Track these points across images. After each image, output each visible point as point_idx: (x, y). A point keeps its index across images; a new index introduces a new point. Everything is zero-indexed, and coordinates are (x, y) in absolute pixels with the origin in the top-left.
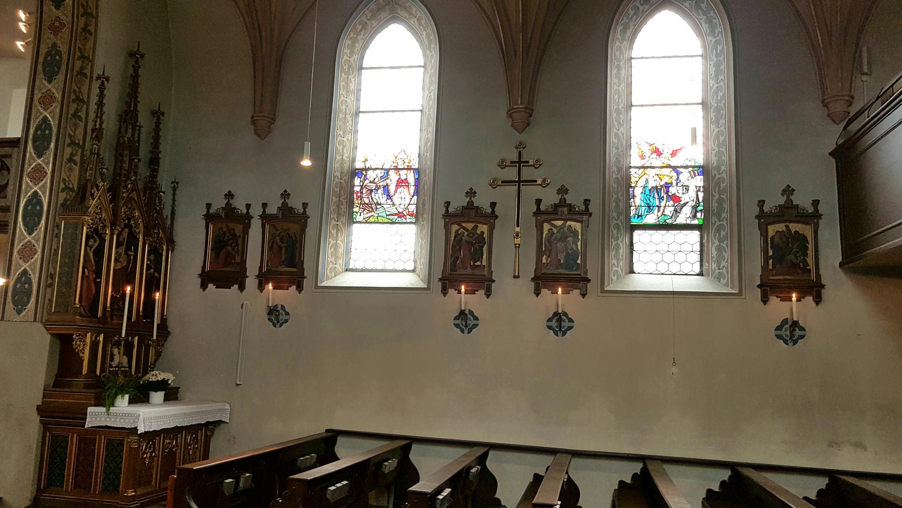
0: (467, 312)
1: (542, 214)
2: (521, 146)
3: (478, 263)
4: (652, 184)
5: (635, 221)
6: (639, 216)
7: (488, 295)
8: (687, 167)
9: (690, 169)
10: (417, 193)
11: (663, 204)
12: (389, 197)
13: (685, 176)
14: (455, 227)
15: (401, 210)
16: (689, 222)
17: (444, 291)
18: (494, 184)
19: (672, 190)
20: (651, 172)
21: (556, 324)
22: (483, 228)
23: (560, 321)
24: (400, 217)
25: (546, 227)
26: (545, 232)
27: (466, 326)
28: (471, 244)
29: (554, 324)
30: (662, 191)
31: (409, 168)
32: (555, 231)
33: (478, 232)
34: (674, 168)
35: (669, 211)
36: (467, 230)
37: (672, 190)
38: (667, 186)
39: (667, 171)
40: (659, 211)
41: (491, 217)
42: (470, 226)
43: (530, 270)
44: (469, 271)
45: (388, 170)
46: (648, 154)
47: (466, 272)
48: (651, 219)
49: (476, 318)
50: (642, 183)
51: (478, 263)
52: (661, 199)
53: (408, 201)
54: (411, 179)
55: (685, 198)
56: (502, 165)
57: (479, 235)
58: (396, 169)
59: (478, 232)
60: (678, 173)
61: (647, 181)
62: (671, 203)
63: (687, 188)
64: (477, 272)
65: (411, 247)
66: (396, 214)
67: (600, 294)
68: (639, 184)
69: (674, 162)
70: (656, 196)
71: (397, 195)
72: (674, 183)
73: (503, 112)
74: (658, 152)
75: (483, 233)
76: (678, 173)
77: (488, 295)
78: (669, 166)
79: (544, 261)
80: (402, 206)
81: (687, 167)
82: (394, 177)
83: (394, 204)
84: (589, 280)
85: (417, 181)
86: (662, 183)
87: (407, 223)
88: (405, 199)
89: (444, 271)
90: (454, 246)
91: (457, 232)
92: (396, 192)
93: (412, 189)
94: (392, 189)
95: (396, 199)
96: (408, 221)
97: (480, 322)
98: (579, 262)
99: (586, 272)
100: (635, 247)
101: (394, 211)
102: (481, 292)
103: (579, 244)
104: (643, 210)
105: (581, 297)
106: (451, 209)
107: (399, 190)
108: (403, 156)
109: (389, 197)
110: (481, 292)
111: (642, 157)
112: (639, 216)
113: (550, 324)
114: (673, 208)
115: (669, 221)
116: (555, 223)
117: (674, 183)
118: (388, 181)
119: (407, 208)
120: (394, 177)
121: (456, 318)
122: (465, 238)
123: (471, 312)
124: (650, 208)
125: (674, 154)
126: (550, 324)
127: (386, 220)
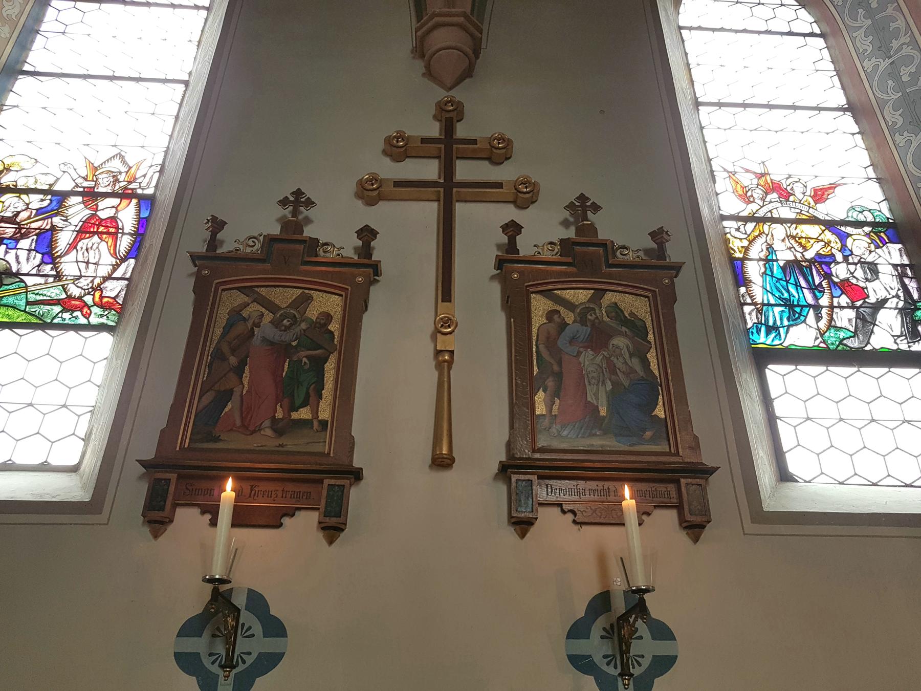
0: (240, 601)
1: (516, 275)
2: (449, 116)
3: (304, 414)
4: (784, 255)
5: (763, 340)
6: (769, 330)
7: (333, 529)
8: (858, 224)
9: (867, 229)
10: (135, 251)
11: (824, 301)
12: (49, 255)
13: (859, 243)
14: (232, 300)
15: (75, 291)
16: (904, 346)
17: (157, 516)
18: (371, 191)
19: (840, 271)
20: (779, 231)
21: (607, 648)
22: (327, 304)
23: (620, 634)
24: (71, 310)
25: (540, 306)
26: (538, 320)
27: (229, 664)
28: (282, 350)
29: (596, 646)
30: (810, 270)
31: (126, 195)
32: (569, 317)
33: (313, 313)
34: (831, 225)
35: (845, 318)
36: (272, 307)
37: (840, 271)
38: (824, 261)
39: (812, 231)
40: (818, 318)
41: (360, 272)
42: (284, 297)
43: (486, 433)
44: (266, 438)
45: (60, 198)
46: (758, 194)
47: (254, 442)
48: (802, 336)
49: (275, 628)
50: (757, 251)
51: (304, 414)
52: (815, 289)
53: (103, 271)
54: (128, 216)
55: (875, 291)
56: (399, 148)
57: (314, 325)
58: (91, 196)
59: (313, 313)
60: (843, 237)
61: (770, 248)
62: (844, 300)
63: (873, 269)
64: (292, 443)
65: (89, 396)
66: (57, 302)
67: (749, 527)
68: (754, 253)
69: (824, 211)
70: (803, 283)
71: (72, 256)
72: (839, 257)
73: (408, 44)
74: (785, 195)
75: (328, 317)
76: (843, 237)
77: (333, 529)
78: (813, 221)
79: (540, 409)
80: (83, 282)
81: (858, 224)
82: (77, 211)
83: (58, 277)
84: (711, 471)
85: (142, 224)
86: (809, 255)
87: (89, 327)
88: (95, 264)
89: (166, 436)
90: (219, 356)
91: (236, 316)
92: (73, 246)
93: (125, 243)
94: (64, 239)
95: (69, 267)
96: (94, 320)
97: (291, 645)
98: (660, 412)
99: (695, 446)
100: (779, 408)
101: (56, 293)
102: (306, 522)
103: (652, 356)
104: (776, 314)
105: (683, 537)
106: (230, 241)
107: (82, 244)
108: (116, 165)
109: (49, 255)
110: (306, 522)
111: (747, 198)
112: (769, 330)
113: (582, 647)
114: (851, 314)
115: (854, 343)
116: (567, 294)
117: (839, 257)
118: (57, 220)
119: (99, 288)
120: (77, 211)
121: (190, 629)
122: (267, 329)
123: (257, 602)
124: (795, 312)
125: (820, 195)
126: (582, 647)
127: (22, 318)
